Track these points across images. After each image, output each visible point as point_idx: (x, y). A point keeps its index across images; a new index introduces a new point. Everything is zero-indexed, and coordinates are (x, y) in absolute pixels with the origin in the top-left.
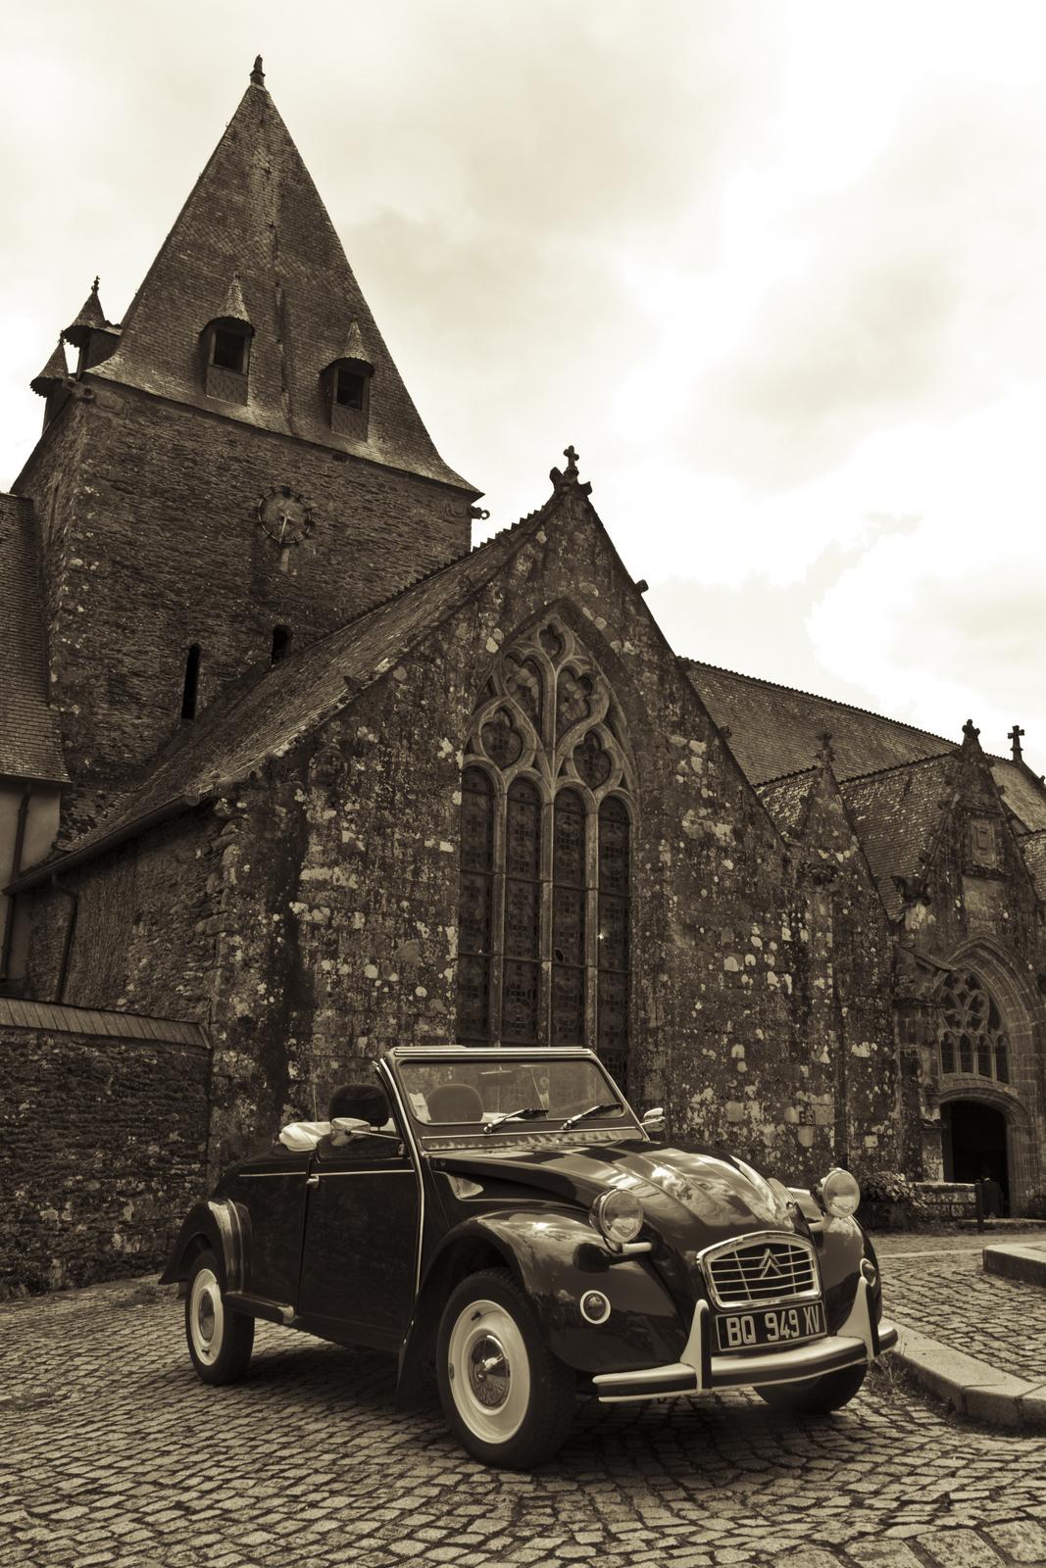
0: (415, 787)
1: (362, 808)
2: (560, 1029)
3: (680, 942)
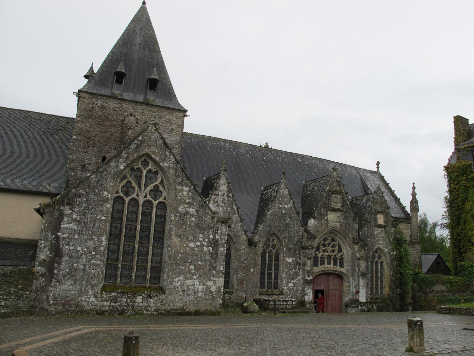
1: (79, 209)
3: (175, 239)
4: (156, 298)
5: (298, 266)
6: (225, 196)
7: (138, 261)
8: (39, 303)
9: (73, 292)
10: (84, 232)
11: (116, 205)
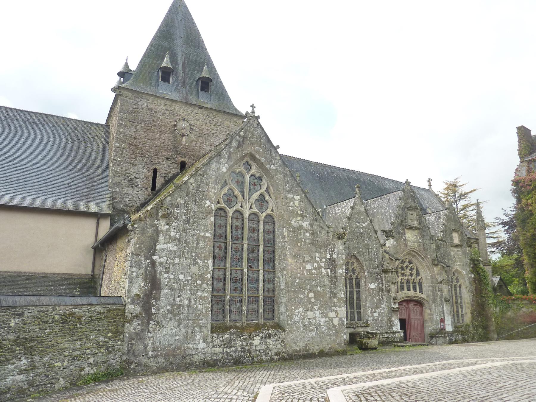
0: (197, 216)
1: (178, 224)
2: (251, 290)
3: (290, 261)
4: (276, 338)
5: (381, 293)
7: (248, 290)
8: (135, 356)
9: (177, 338)
10: (186, 254)
11: (217, 219)
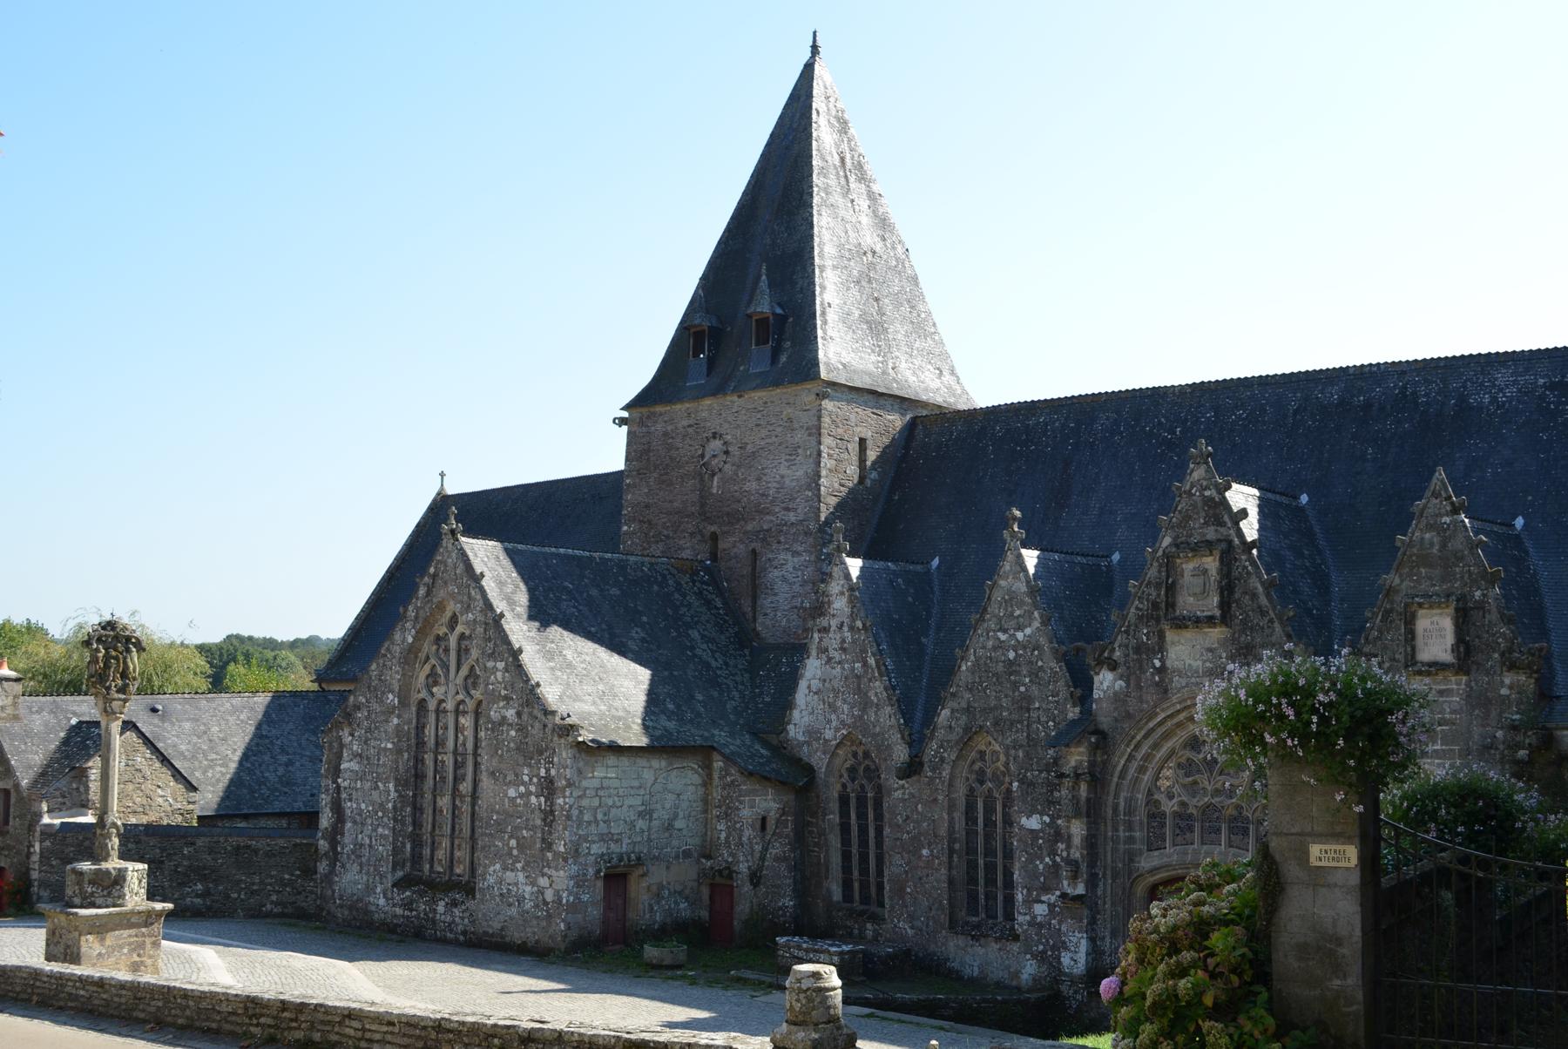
6: (846, 629)
